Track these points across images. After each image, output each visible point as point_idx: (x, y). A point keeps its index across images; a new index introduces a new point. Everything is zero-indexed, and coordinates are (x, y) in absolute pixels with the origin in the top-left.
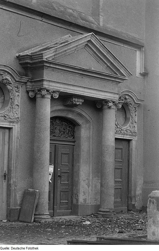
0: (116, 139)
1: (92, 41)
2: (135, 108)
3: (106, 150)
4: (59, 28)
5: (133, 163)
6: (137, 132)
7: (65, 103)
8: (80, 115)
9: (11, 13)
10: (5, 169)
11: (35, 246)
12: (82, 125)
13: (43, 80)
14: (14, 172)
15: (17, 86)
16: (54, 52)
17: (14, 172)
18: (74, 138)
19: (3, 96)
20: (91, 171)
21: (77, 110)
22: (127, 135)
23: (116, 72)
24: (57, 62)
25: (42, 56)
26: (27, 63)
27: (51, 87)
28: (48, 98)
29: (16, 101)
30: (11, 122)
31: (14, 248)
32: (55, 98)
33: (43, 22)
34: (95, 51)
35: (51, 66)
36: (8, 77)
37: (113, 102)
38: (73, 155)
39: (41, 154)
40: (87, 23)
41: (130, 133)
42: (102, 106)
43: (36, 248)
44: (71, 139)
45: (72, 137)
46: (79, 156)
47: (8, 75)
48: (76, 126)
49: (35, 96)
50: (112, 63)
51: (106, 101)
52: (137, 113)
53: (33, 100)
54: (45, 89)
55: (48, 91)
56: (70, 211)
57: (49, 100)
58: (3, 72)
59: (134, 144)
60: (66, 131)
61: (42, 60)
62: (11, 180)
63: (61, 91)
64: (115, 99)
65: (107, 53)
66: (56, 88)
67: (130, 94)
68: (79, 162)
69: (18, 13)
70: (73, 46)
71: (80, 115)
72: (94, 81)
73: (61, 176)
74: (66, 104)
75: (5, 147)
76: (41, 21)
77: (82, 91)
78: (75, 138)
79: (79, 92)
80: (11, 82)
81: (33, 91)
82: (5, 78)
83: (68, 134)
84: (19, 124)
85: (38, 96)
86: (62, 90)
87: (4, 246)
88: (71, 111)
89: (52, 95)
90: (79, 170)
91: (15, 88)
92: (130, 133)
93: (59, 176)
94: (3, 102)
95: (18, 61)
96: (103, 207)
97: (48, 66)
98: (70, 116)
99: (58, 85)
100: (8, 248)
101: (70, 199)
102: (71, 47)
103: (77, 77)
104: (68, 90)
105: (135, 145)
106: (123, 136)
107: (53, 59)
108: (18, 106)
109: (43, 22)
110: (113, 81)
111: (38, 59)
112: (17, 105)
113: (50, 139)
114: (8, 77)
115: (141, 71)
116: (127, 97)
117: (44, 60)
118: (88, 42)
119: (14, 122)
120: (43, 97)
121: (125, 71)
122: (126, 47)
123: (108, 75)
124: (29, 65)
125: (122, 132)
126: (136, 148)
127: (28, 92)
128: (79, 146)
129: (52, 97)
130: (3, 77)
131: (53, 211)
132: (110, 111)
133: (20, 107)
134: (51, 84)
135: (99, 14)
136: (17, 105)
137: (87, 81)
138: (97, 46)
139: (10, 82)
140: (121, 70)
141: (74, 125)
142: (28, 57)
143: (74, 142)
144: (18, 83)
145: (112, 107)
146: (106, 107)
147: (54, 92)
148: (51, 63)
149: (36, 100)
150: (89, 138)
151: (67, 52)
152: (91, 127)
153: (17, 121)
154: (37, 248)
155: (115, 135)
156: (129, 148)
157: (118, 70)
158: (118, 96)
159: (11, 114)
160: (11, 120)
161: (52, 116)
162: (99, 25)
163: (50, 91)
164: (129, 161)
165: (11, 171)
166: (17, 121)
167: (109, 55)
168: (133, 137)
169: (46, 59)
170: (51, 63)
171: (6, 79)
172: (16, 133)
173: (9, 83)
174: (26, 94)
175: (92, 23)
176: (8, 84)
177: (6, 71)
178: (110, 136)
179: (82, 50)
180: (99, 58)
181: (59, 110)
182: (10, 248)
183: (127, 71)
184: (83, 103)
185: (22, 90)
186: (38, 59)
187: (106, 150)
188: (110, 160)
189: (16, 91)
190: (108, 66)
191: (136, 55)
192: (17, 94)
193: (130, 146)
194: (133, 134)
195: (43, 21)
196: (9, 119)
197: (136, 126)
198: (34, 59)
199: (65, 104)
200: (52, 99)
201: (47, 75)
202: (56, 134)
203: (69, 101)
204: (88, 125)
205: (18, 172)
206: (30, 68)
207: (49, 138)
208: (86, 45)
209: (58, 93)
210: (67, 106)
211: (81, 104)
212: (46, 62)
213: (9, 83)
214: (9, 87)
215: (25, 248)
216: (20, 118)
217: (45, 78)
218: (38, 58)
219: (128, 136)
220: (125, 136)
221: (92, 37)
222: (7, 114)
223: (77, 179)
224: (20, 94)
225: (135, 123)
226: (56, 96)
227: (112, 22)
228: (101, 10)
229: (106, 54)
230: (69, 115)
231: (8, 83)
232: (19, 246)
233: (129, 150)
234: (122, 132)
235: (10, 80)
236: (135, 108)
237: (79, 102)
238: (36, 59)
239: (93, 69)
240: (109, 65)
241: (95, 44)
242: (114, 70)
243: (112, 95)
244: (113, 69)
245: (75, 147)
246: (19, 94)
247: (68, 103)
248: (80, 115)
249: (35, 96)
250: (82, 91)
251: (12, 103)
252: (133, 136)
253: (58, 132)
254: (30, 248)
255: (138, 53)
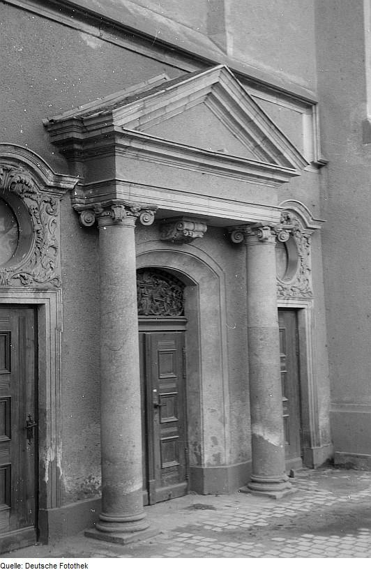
0: (280, 309)
1: (223, 85)
2: (307, 239)
3: (261, 340)
4: (141, 56)
5: (309, 359)
6: (311, 290)
7: (164, 236)
8: (197, 261)
9: (23, 12)
10: (30, 411)
11: (81, 561)
12: (200, 283)
13: (114, 182)
14: (53, 416)
15: (49, 200)
16: (139, 110)
17: (53, 416)
18: (183, 314)
19: (16, 225)
20: (226, 387)
21: (189, 249)
22: (294, 298)
23: (274, 158)
24: (147, 133)
25: (112, 120)
26: (72, 141)
27: (134, 199)
28: (128, 226)
29: (49, 236)
30: (38, 290)
31: (32, 566)
32: (144, 224)
33: (104, 40)
34: (228, 109)
35: (134, 145)
36: (27, 177)
37: (272, 228)
38: (183, 354)
39: (118, 367)
40: (202, 48)
41: (301, 295)
42: (246, 236)
43: (82, 565)
44: (177, 317)
45: (180, 313)
46: (196, 355)
47: (26, 172)
48: (185, 286)
49: (96, 223)
50: (265, 138)
51: (257, 227)
52: (309, 249)
53: (91, 232)
54: (121, 203)
55: (128, 208)
56: (184, 484)
57: (132, 231)
58: (11, 163)
59: (307, 317)
60: (166, 300)
61: (110, 130)
62: (45, 436)
63: (159, 207)
64: (274, 220)
65: (255, 113)
66: (147, 200)
67: (296, 209)
68: (197, 369)
69: (43, 13)
70: (182, 96)
71: (197, 261)
72: (227, 180)
73: (160, 407)
74: (167, 238)
75: (28, 354)
76: (98, 37)
77: (205, 206)
78: (185, 313)
79: (199, 208)
80: (35, 190)
81: (91, 210)
82: (18, 179)
83: (170, 305)
84: (60, 292)
85: (104, 221)
86: (161, 205)
87: (9, 561)
88: (176, 253)
89: (139, 218)
90: (199, 387)
91: (46, 204)
92: (301, 295)
93: (156, 406)
94: (17, 242)
95: (46, 136)
96: (261, 472)
97: (126, 147)
98: (175, 265)
99: (151, 193)
100: (18, 566)
101: (181, 456)
102: (177, 98)
103: (193, 173)
104: (173, 205)
105: (310, 318)
106: (286, 301)
107: (136, 129)
108: (55, 248)
109: (104, 40)
110: (269, 179)
111: (100, 129)
112: (52, 246)
113: (139, 322)
114: (27, 177)
115: (314, 158)
116: (292, 215)
117: (116, 129)
118: (212, 88)
119: (47, 290)
120: (116, 222)
121: (293, 157)
122: (283, 105)
123: (259, 165)
124: (77, 147)
125: (285, 293)
126: (312, 326)
127: (77, 213)
128: (196, 332)
129: (138, 222)
130: (12, 176)
131: (147, 493)
132: (264, 248)
133: (59, 250)
134: (135, 190)
135: (225, 31)
136: (52, 246)
137: (215, 183)
138: (234, 97)
139: (31, 190)
140: (285, 154)
141: (183, 284)
142: (74, 123)
143: (184, 323)
144: (52, 190)
145: (270, 240)
146: (253, 240)
147: (143, 210)
148: (132, 138)
149: (98, 231)
150: (217, 313)
151: (168, 110)
152: (222, 287)
153: (56, 285)
154: (84, 566)
155: (279, 301)
156: (297, 327)
157: (280, 154)
158: (278, 214)
159: (37, 271)
160: (40, 286)
161: (140, 267)
162: (226, 54)
163: (135, 209)
164: (298, 355)
165: (45, 415)
166: (56, 285)
167: (260, 119)
168: (307, 303)
169: (122, 127)
170: (132, 138)
171: (21, 182)
172: (53, 318)
173: (30, 192)
174: (73, 218)
175: (210, 48)
176: (27, 195)
177: (19, 161)
178: (267, 305)
179: (199, 107)
180: (236, 128)
181: (151, 253)
182: (24, 566)
183: (298, 156)
184: (206, 234)
185: (62, 208)
186: (100, 129)
187: (261, 340)
188: (270, 360)
189: (49, 210)
190: (257, 146)
191: (301, 123)
192: (51, 218)
193: (300, 320)
194: (306, 294)
195: (103, 37)
196: (34, 284)
197: (310, 279)
198: (89, 129)
199: (164, 239)
200: (139, 225)
201: (125, 167)
202: (144, 308)
203: (175, 232)
204: (213, 284)
205: (64, 414)
206: (80, 152)
207: (137, 320)
208: (208, 94)
209: (152, 212)
210: (168, 242)
211: (201, 236)
212: (122, 136)
213: (30, 192)
214: (28, 202)
215: (58, 566)
216: (60, 280)
217: (120, 175)
218: (101, 126)
219: (297, 302)
220: (290, 301)
221: (223, 77)
222: (29, 270)
223: (194, 410)
224: (57, 219)
225: (307, 272)
226: (149, 219)
227: (252, 48)
228: (227, 21)
229: (252, 118)
230: (173, 263)
231: (27, 192)
232: (45, 561)
233: (297, 332)
234: (285, 293)
235: (32, 184)
236: (307, 239)
237: (196, 230)
238: (94, 128)
239: (226, 152)
240: (259, 143)
241: (230, 92)
242: (271, 155)
243: (267, 212)
244: (268, 152)
245: (186, 334)
246: (54, 218)
247: (170, 237)
248: (196, 261)
249: (96, 223)
250: (205, 206)
251: (40, 243)
252: (305, 299)
253: (149, 302)
254: (68, 566)
255: (305, 118)
